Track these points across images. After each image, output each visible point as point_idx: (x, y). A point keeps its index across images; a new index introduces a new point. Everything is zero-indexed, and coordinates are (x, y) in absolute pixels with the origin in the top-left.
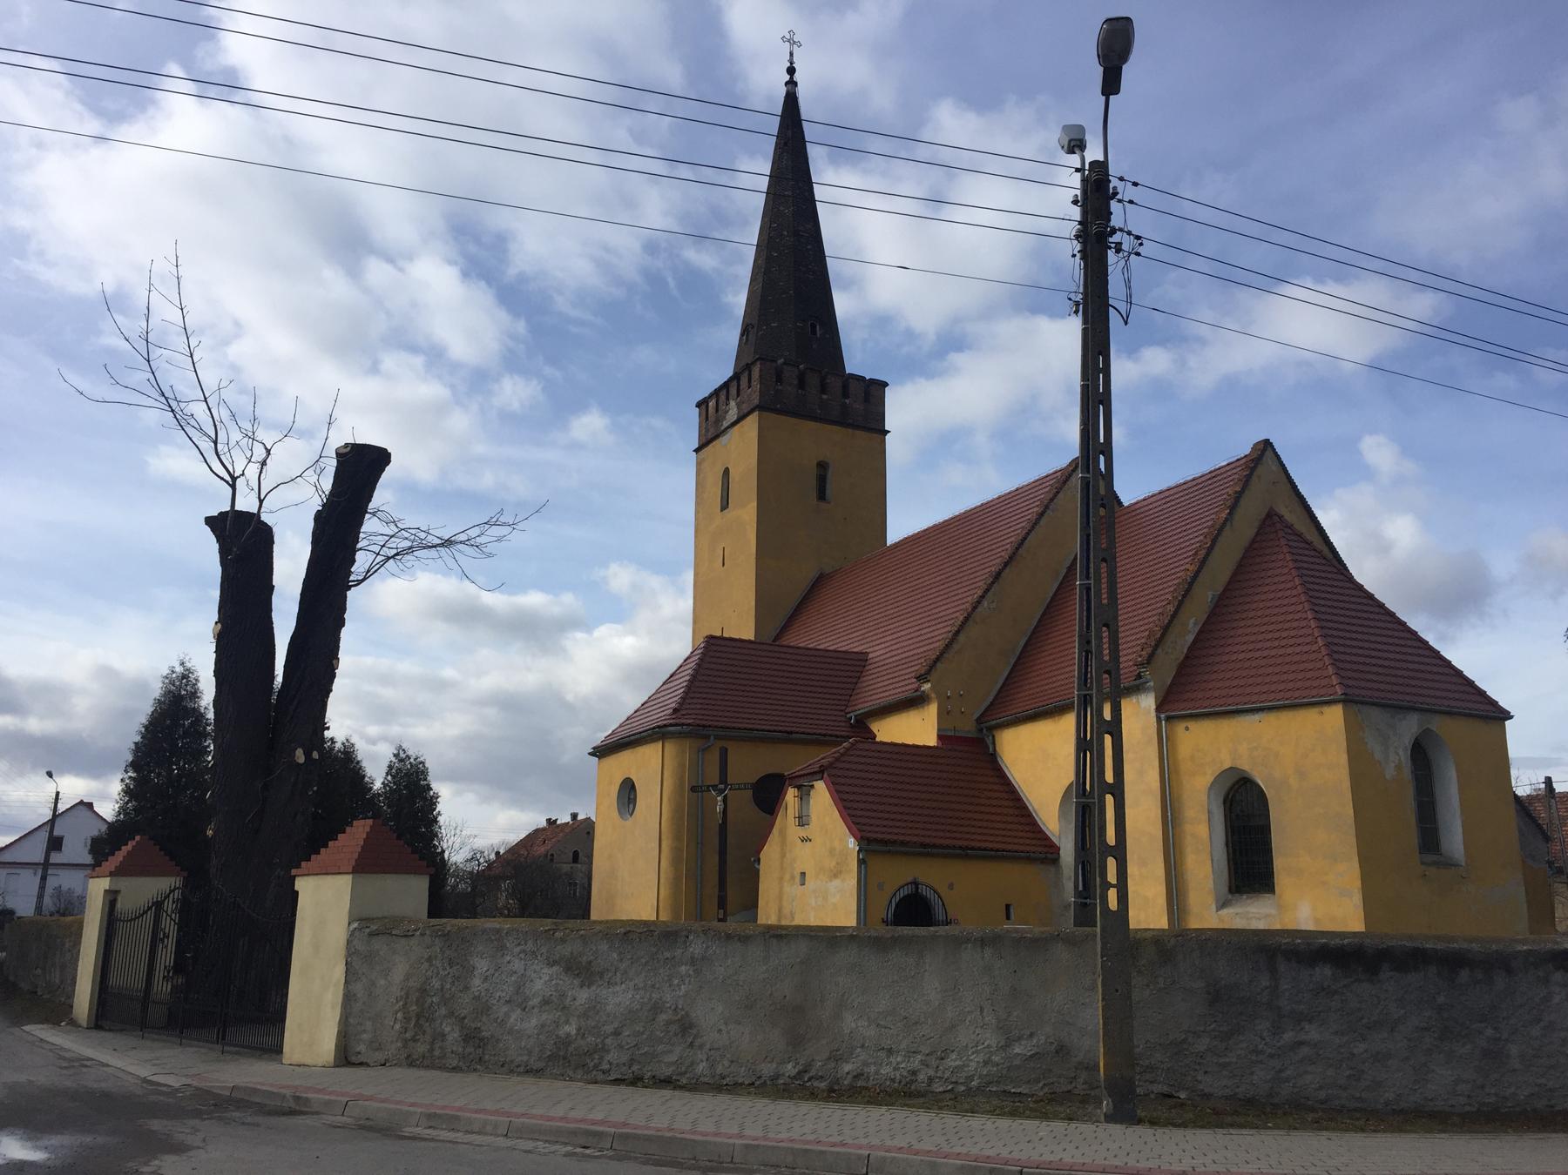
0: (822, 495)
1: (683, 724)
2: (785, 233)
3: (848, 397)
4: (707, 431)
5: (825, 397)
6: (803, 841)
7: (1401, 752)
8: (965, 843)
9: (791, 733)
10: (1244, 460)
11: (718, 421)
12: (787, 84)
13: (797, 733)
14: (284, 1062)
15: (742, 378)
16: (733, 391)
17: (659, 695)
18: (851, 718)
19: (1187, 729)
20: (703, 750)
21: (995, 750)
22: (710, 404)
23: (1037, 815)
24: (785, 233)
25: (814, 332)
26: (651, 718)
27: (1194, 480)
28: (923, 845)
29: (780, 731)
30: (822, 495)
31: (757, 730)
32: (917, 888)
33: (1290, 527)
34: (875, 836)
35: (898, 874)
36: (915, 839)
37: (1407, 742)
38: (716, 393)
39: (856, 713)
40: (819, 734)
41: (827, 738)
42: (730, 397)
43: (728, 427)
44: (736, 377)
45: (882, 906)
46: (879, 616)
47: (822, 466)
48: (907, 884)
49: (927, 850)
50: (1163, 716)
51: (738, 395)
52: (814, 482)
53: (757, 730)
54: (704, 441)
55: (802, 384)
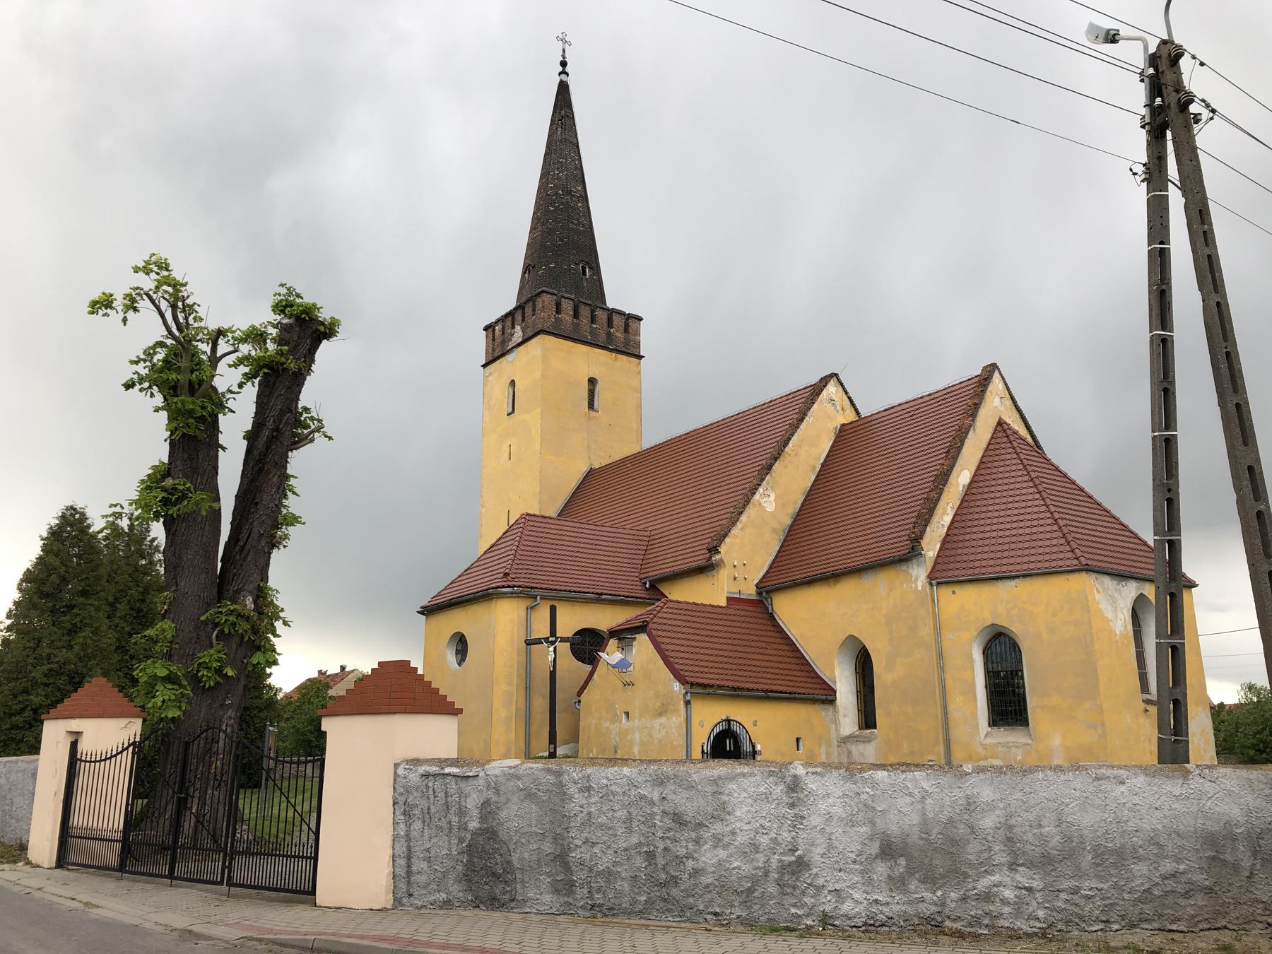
0: (591, 406)
1: (514, 586)
2: (560, 192)
3: (612, 327)
4: (494, 350)
5: (595, 326)
6: (625, 685)
7: (1125, 612)
8: (767, 687)
9: (602, 594)
10: (977, 379)
11: (504, 342)
12: (560, 74)
13: (606, 594)
14: (318, 902)
15: (516, 316)
16: (518, 317)
17: (479, 563)
18: (645, 583)
19: (954, 592)
20: (531, 608)
21: (772, 610)
22: (497, 328)
23: (815, 664)
24: (560, 192)
25: (584, 273)
26: (482, 581)
27: (930, 395)
28: (734, 689)
29: (593, 593)
30: (591, 406)
31: (574, 592)
32: (729, 724)
33: (1016, 433)
34: (698, 680)
35: (709, 716)
36: (727, 683)
37: (1129, 605)
38: (502, 319)
39: (650, 579)
40: (624, 596)
41: (629, 599)
42: (516, 323)
43: (514, 347)
44: (520, 307)
45: (702, 737)
46: (937, 458)
47: (592, 382)
48: (719, 723)
49: (737, 693)
50: (934, 582)
51: (523, 320)
52: (586, 395)
53: (574, 592)
54: (491, 358)
55: (576, 315)
